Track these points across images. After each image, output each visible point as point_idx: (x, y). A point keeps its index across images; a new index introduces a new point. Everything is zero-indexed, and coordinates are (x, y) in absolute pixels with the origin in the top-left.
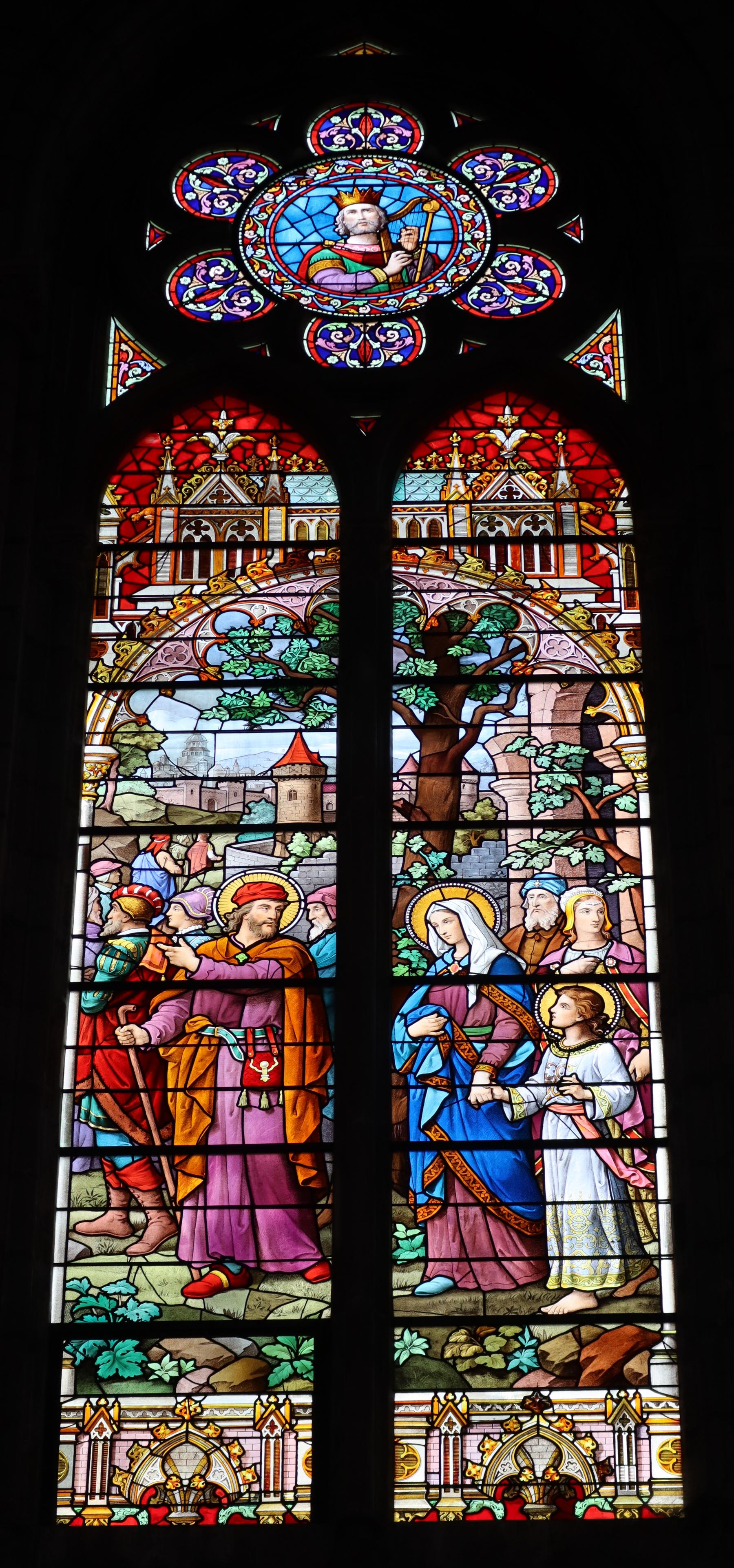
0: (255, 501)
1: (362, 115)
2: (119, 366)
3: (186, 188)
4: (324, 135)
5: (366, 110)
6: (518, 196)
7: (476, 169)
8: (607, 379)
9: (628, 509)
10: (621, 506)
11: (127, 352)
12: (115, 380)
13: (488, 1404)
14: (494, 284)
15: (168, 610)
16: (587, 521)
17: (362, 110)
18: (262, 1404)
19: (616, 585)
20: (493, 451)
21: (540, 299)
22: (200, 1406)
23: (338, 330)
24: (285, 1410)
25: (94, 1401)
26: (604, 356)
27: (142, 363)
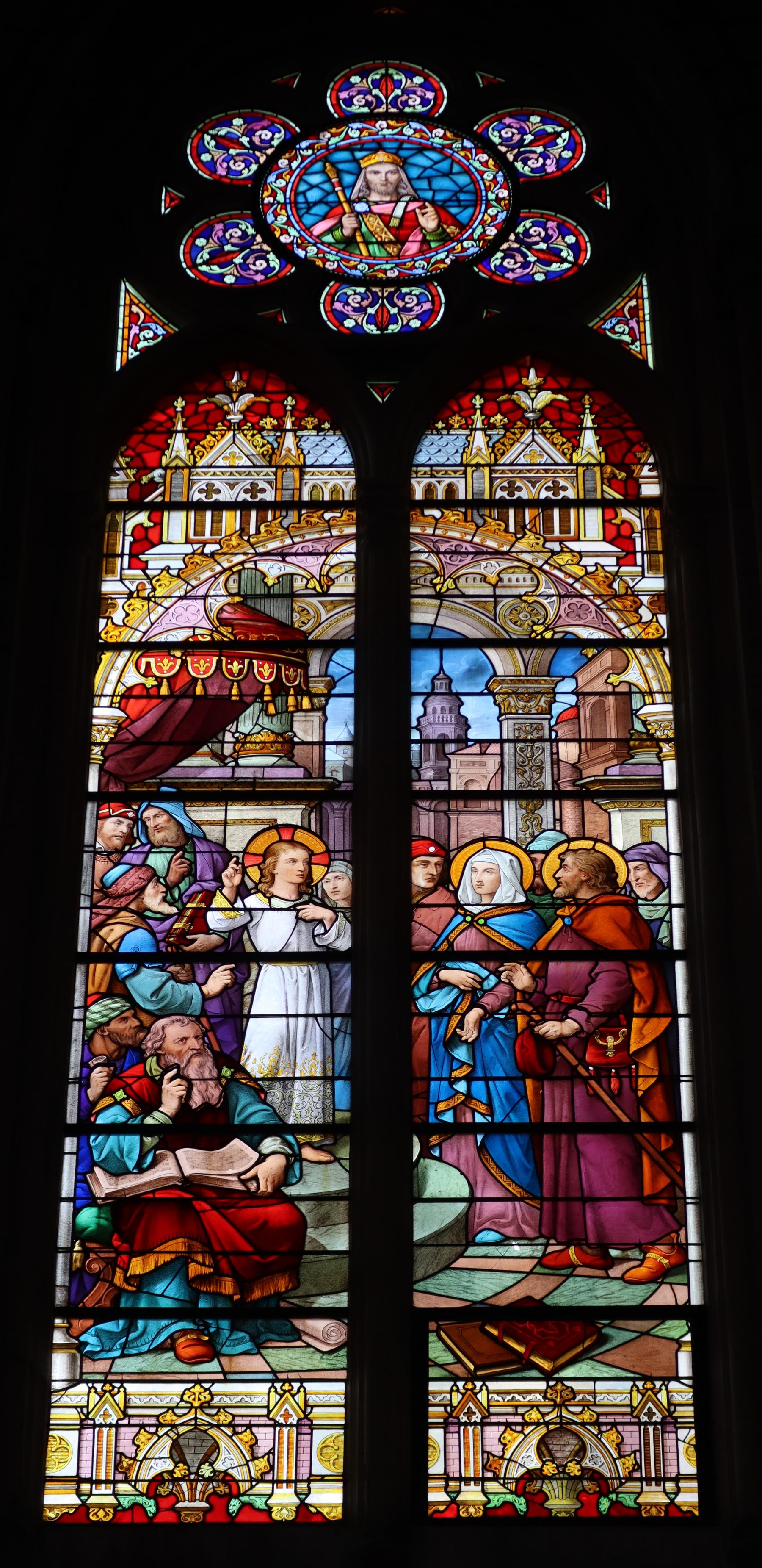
0: (270, 462)
1: (383, 76)
2: (130, 328)
3: (201, 148)
4: (344, 95)
5: (387, 71)
6: (545, 160)
7: (503, 132)
8: (633, 343)
9: (655, 473)
10: (645, 471)
11: (138, 315)
12: (126, 342)
13: (238, 1395)
14: (518, 250)
15: (180, 570)
16: (610, 486)
17: (383, 71)
18: (276, 1391)
19: (638, 548)
20: (515, 412)
21: (566, 266)
22: (210, 1393)
23: (356, 294)
24: (662, 1397)
25: (99, 1386)
26: (633, 327)
27: (153, 326)
